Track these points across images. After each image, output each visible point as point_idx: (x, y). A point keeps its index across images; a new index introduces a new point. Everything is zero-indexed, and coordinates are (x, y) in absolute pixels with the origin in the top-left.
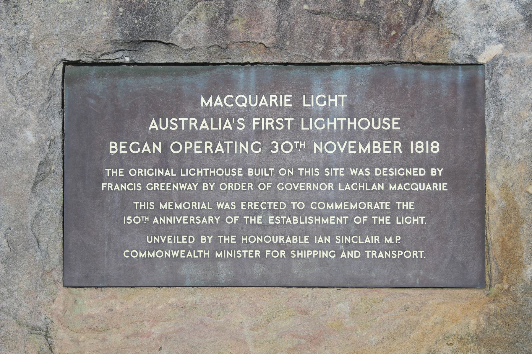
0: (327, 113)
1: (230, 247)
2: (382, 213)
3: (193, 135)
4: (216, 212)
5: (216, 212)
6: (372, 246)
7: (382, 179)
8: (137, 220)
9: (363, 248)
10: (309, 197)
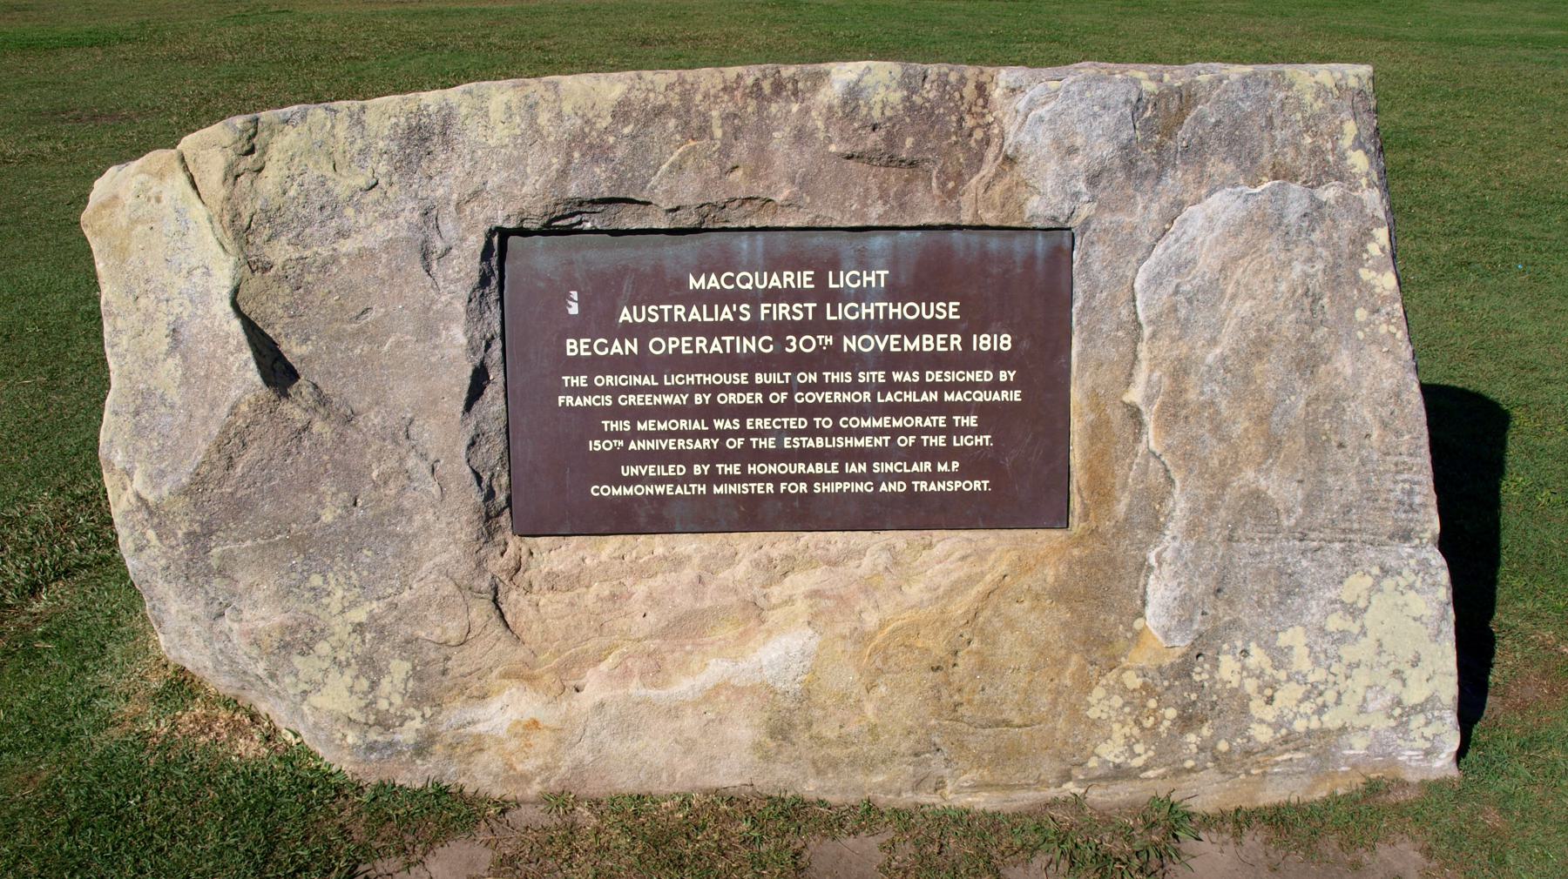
0: (862, 296)
2: (935, 431)
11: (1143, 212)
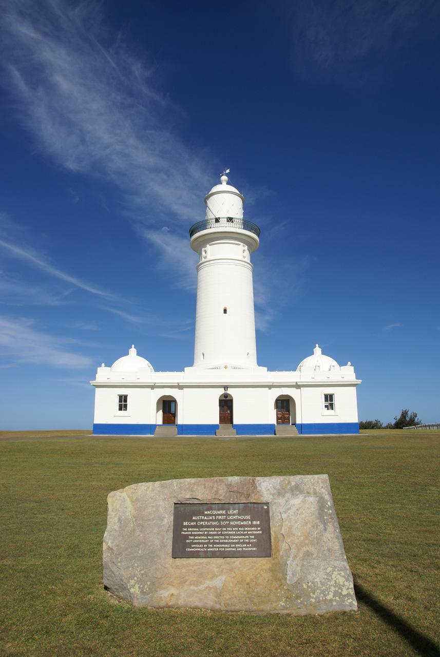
0: (234, 515)
1: (211, 548)
2: (247, 539)
3: (203, 520)
4: (208, 539)
5: (208, 539)
6: (244, 547)
7: (246, 531)
8: (189, 541)
9: (242, 547)
10: (229, 535)
11: (281, 501)
